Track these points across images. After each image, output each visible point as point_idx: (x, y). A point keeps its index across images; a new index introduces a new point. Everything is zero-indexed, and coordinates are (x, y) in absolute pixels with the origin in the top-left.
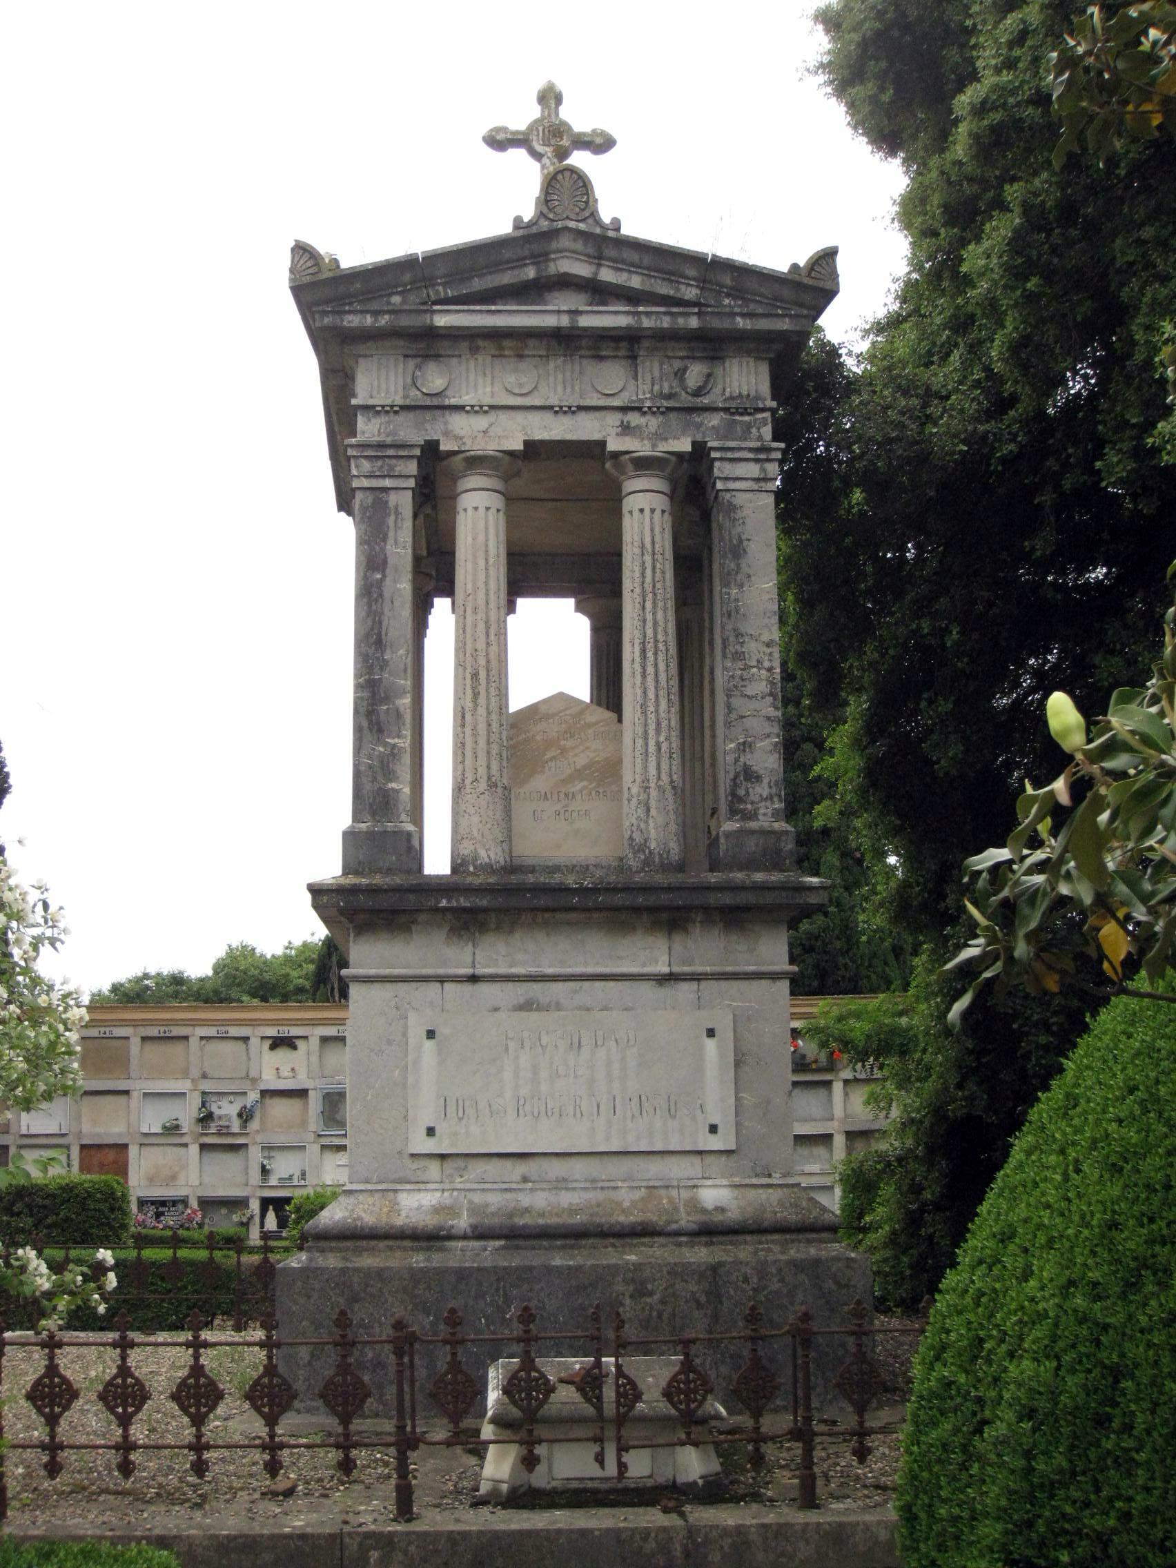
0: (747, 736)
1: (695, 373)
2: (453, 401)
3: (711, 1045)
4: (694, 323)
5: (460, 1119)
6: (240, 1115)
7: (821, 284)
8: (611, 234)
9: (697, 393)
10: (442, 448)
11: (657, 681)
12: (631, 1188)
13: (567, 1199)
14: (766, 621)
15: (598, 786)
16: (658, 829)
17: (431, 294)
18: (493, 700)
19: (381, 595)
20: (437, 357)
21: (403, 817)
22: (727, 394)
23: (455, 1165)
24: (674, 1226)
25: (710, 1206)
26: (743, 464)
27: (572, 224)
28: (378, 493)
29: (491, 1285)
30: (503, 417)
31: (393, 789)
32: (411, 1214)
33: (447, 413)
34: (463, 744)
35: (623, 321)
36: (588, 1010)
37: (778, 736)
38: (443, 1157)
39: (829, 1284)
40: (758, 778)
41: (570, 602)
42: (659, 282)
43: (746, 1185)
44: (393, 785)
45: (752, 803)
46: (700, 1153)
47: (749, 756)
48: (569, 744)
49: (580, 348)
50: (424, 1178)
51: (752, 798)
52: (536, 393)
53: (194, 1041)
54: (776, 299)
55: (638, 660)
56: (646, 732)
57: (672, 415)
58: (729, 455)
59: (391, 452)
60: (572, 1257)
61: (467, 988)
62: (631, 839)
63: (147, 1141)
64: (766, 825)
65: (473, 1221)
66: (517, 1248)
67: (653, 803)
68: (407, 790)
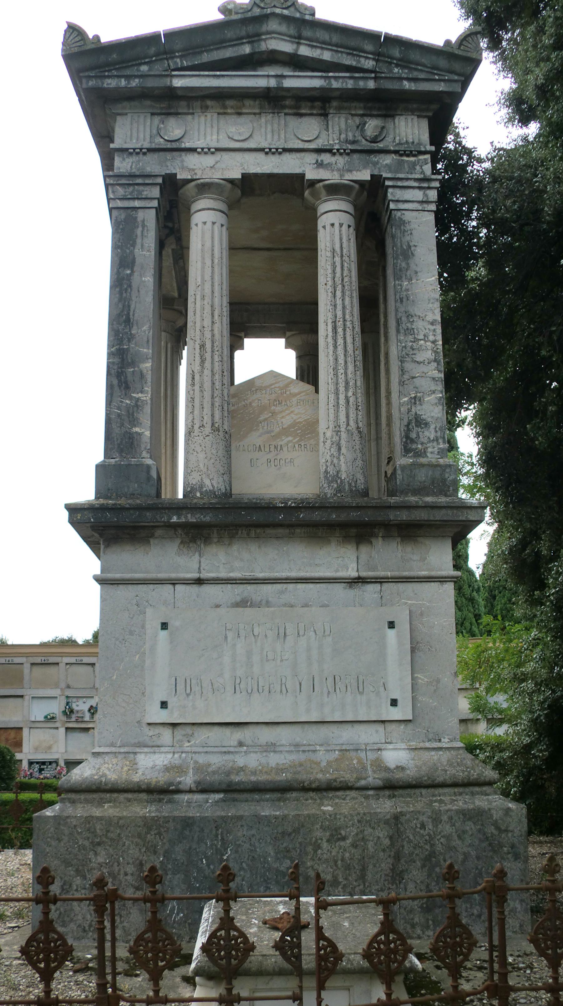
0: (416, 392)
1: (372, 125)
2: (188, 145)
3: (391, 633)
4: (371, 85)
5: (188, 695)
6: (89, 710)
7: (469, 55)
8: (307, 17)
9: (374, 140)
10: (179, 177)
11: (346, 351)
12: (327, 751)
13: (274, 760)
14: (431, 305)
15: (301, 440)
16: (347, 464)
17: (171, 64)
18: (216, 364)
19: (130, 286)
20: (177, 114)
21: (144, 454)
22: (397, 142)
23: (184, 733)
24: (363, 783)
25: (392, 765)
26: (411, 191)
27: (278, 11)
28: (129, 211)
29: (211, 831)
30: (226, 156)
31: (136, 432)
32: (146, 773)
33: (183, 154)
34: (193, 399)
35: (317, 83)
36: (292, 606)
37: (442, 392)
38: (174, 725)
39: (491, 830)
40: (427, 424)
41: (282, 341)
42: (344, 55)
43: (421, 748)
44: (137, 429)
45: (422, 444)
46: (383, 722)
47: (419, 407)
48: (278, 409)
49: (284, 107)
50: (159, 743)
51: (422, 440)
52: (251, 139)
53: (62, 665)
54: (433, 68)
55: (330, 334)
56: (337, 389)
57: (356, 156)
58: (400, 184)
59: (140, 181)
60: (280, 808)
61: (195, 589)
62: (326, 472)
63: (34, 725)
64: (433, 460)
65: (197, 778)
66: (234, 800)
67: (343, 443)
68: (148, 433)
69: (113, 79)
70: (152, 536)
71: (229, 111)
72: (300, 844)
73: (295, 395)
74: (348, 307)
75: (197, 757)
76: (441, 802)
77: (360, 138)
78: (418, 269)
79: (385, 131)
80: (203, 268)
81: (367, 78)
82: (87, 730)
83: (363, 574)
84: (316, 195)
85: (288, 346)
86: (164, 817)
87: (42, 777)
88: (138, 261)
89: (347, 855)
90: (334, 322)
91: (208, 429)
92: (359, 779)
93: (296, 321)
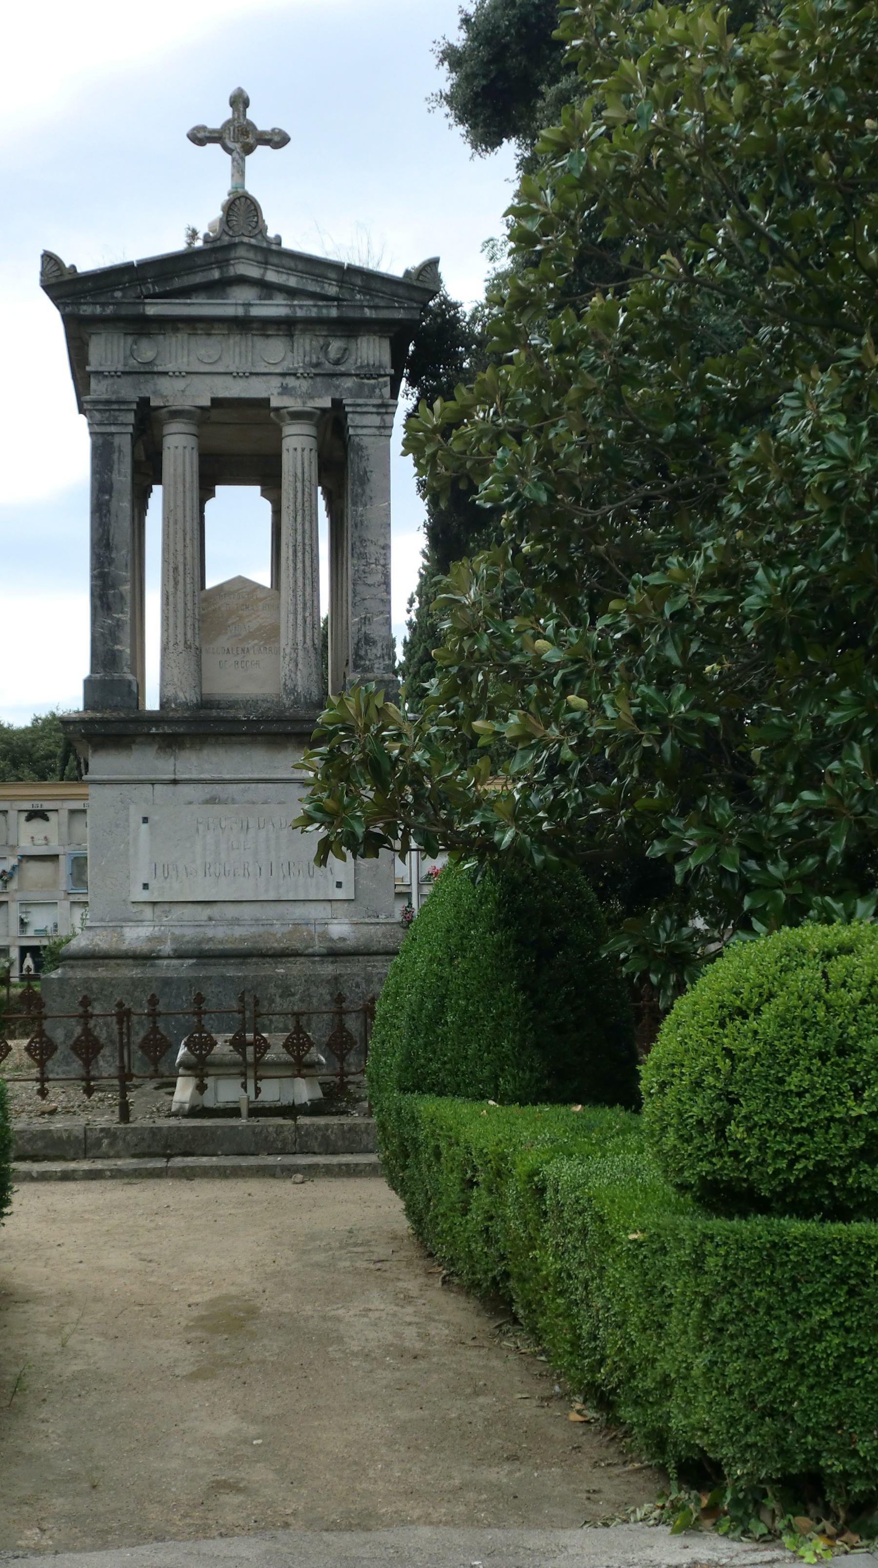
1: (335, 346)
2: (160, 369)
4: (334, 313)
7: (426, 286)
8: (274, 247)
9: (337, 362)
11: (304, 573)
13: (238, 932)
18: (188, 586)
19: (109, 511)
21: (126, 669)
27: (246, 240)
30: (196, 379)
40: (374, 643)
49: (252, 329)
55: (291, 558)
57: (318, 379)
58: (359, 409)
61: (171, 787)
62: (285, 684)
65: (174, 947)
66: (204, 965)
67: (300, 660)
70: (134, 742)
73: (261, 600)
76: (374, 966)
88: (116, 486)
90: (295, 546)
91: (181, 647)
92: (307, 948)
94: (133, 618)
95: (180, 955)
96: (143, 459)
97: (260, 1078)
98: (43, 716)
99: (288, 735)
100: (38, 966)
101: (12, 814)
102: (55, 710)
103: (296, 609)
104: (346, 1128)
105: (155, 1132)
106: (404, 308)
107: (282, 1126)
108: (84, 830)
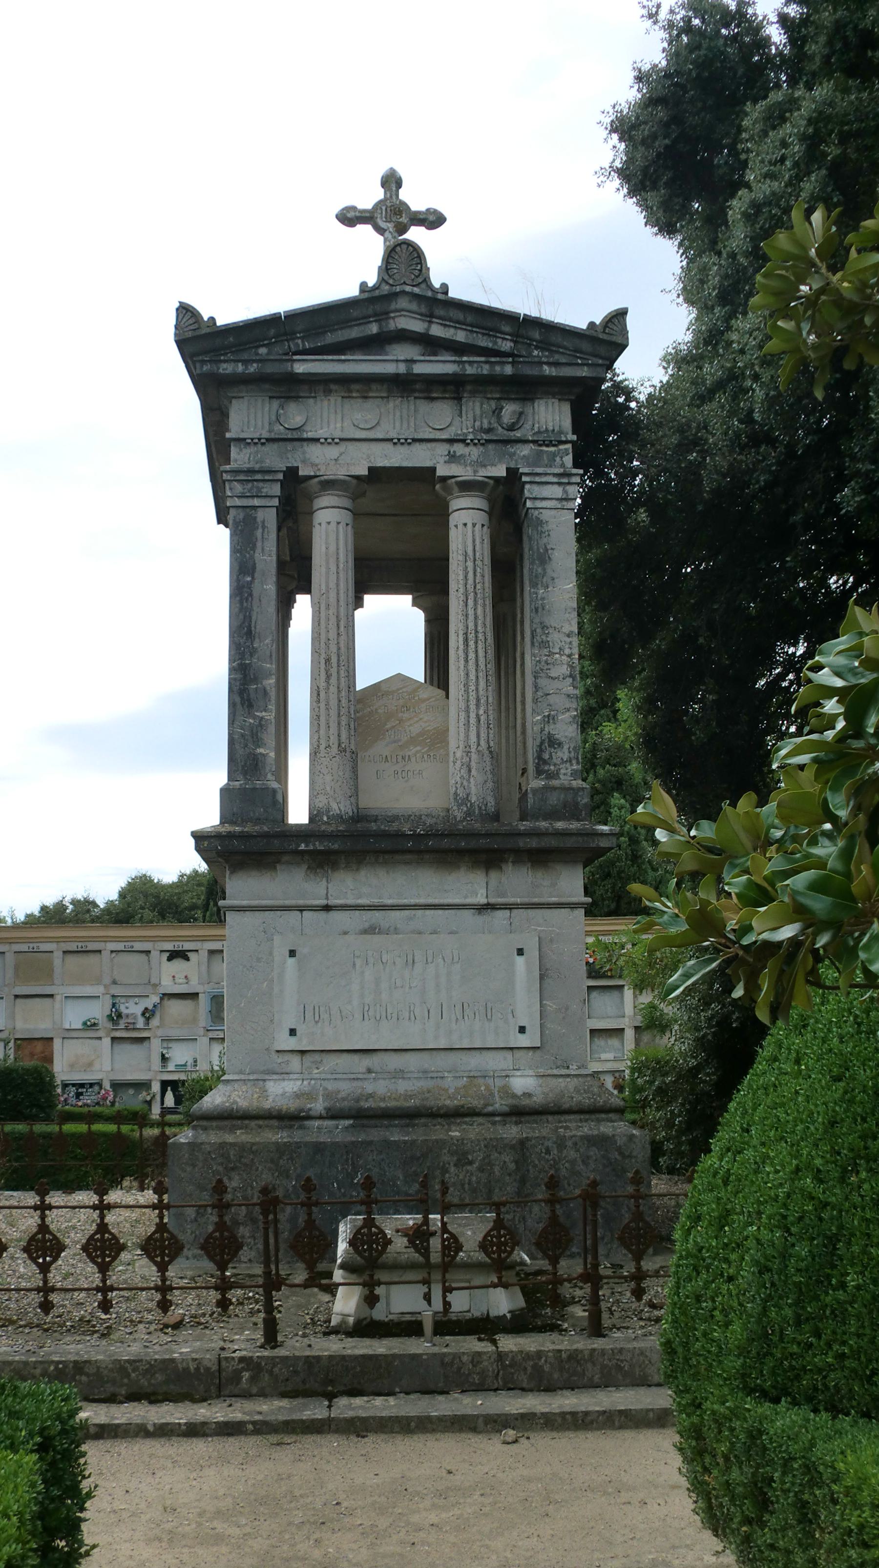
1: (509, 410)
2: (310, 435)
3: (520, 961)
4: (508, 370)
5: (317, 1022)
6: (143, 1014)
7: (614, 339)
8: (440, 296)
9: (511, 428)
11: (477, 665)
12: (456, 1077)
13: (403, 1087)
14: (567, 615)
16: (478, 788)
18: (343, 680)
19: (251, 595)
21: (269, 776)
22: (536, 430)
24: (490, 1109)
27: (408, 289)
30: (351, 446)
31: (261, 754)
33: (305, 444)
34: (318, 717)
35: (449, 369)
38: (303, 1052)
40: (560, 744)
45: (555, 765)
46: (511, 1049)
47: (552, 727)
48: (406, 715)
49: (414, 391)
52: (378, 428)
53: (106, 954)
54: (575, 351)
55: (461, 647)
57: (490, 447)
58: (537, 479)
60: (408, 1134)
61: (323, 915)
62: (456, 794)
63: (68, 1034)
64: (566, 783)
65: (326, 1104)
66: (363, 1126)
67: (473, 764)
69: (227, 361)
70: (279, 862)
71: (354, 395)
72: (429, 1168)
73: (424, 701)
74: (481, 617)
75: (326, 1084)
76: (566, 1128)
77: (496, 425)
78: (554, 575)
79: (523, 417)
80: (327, 573)
81: (504, 363)
82: (141, 1040)
83: (492, 900)
84: (448, 490)
85: (415, 604)
86: (296, 1143)
87: (80, 1104)
88: (259, 567)
89: (474, 1179)
90: (466, 634)
91: (334, 750)
92: (486, 1105)
93: (425, 580)
94: (277, 718)
95: (333, 1115)
96: (288, 558)
97: (450, 1290)
98: (188, 873)
99: (461, 853)
100: (178, 1100)
101: (155, 954)
102: (197, 868)
103: (468, 706)
104: (564, 1355)
105: (311, 1362)
106: (588, 365)
107: (479, 1354)
108: (223, 968)
